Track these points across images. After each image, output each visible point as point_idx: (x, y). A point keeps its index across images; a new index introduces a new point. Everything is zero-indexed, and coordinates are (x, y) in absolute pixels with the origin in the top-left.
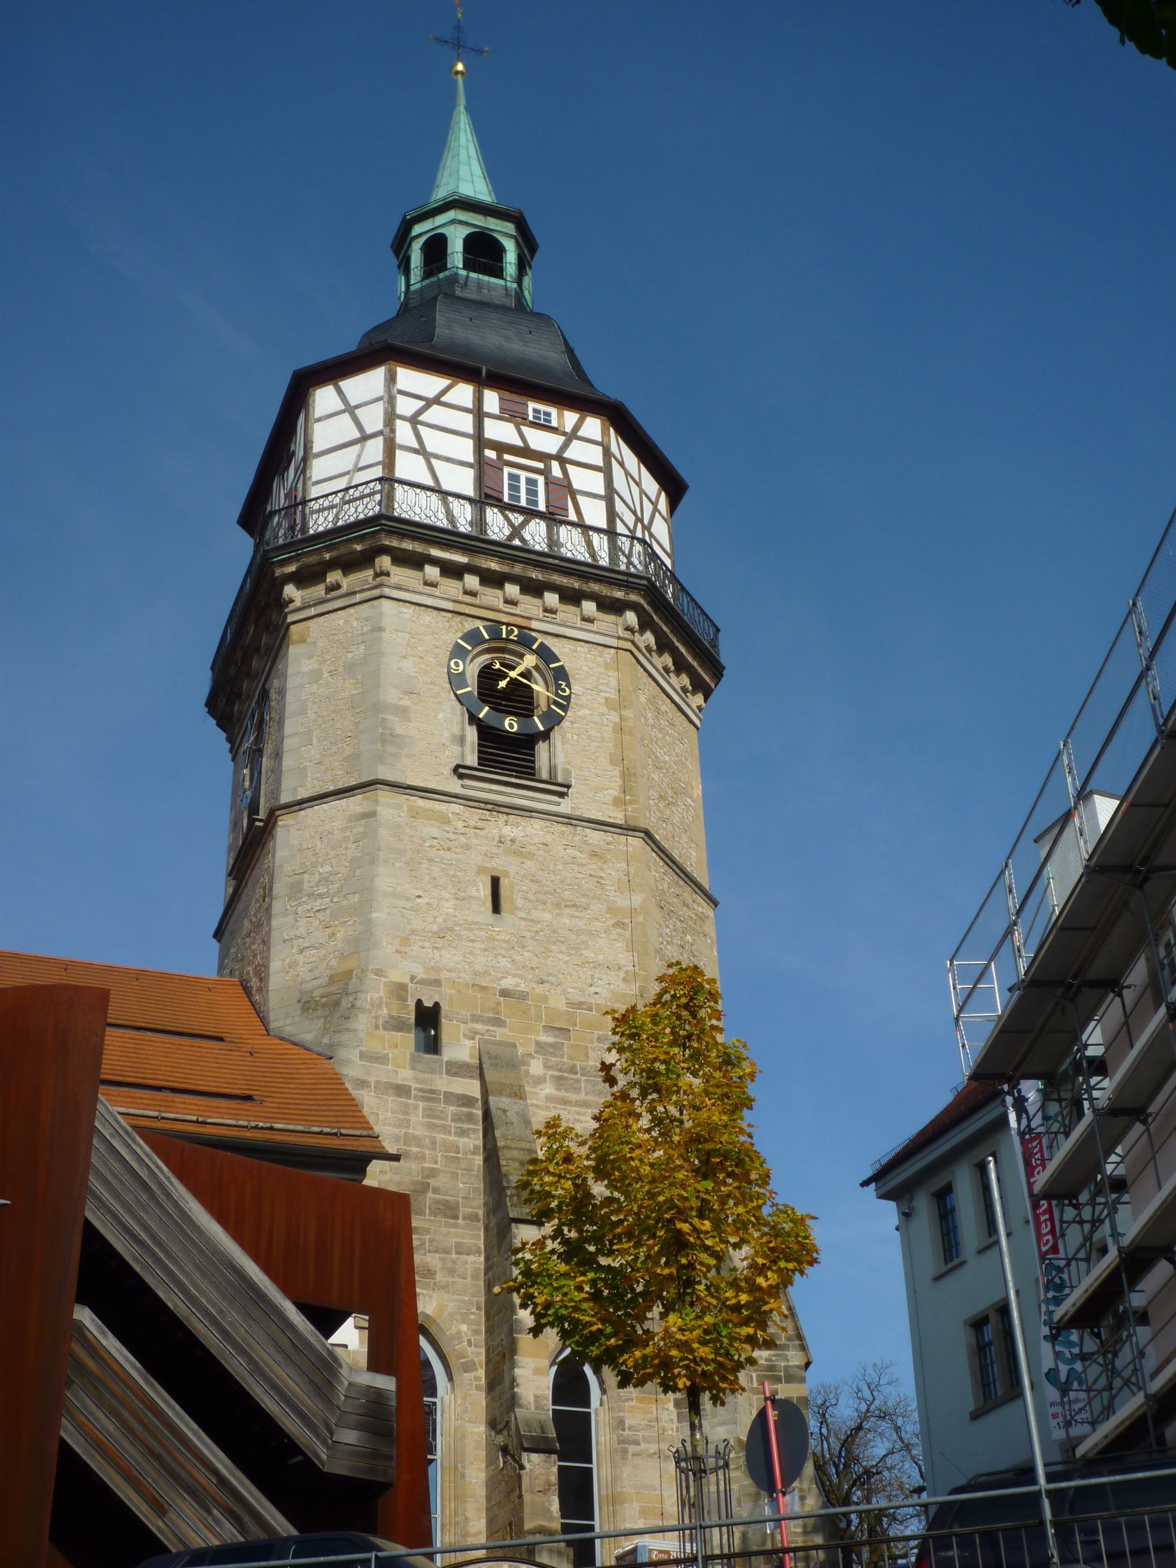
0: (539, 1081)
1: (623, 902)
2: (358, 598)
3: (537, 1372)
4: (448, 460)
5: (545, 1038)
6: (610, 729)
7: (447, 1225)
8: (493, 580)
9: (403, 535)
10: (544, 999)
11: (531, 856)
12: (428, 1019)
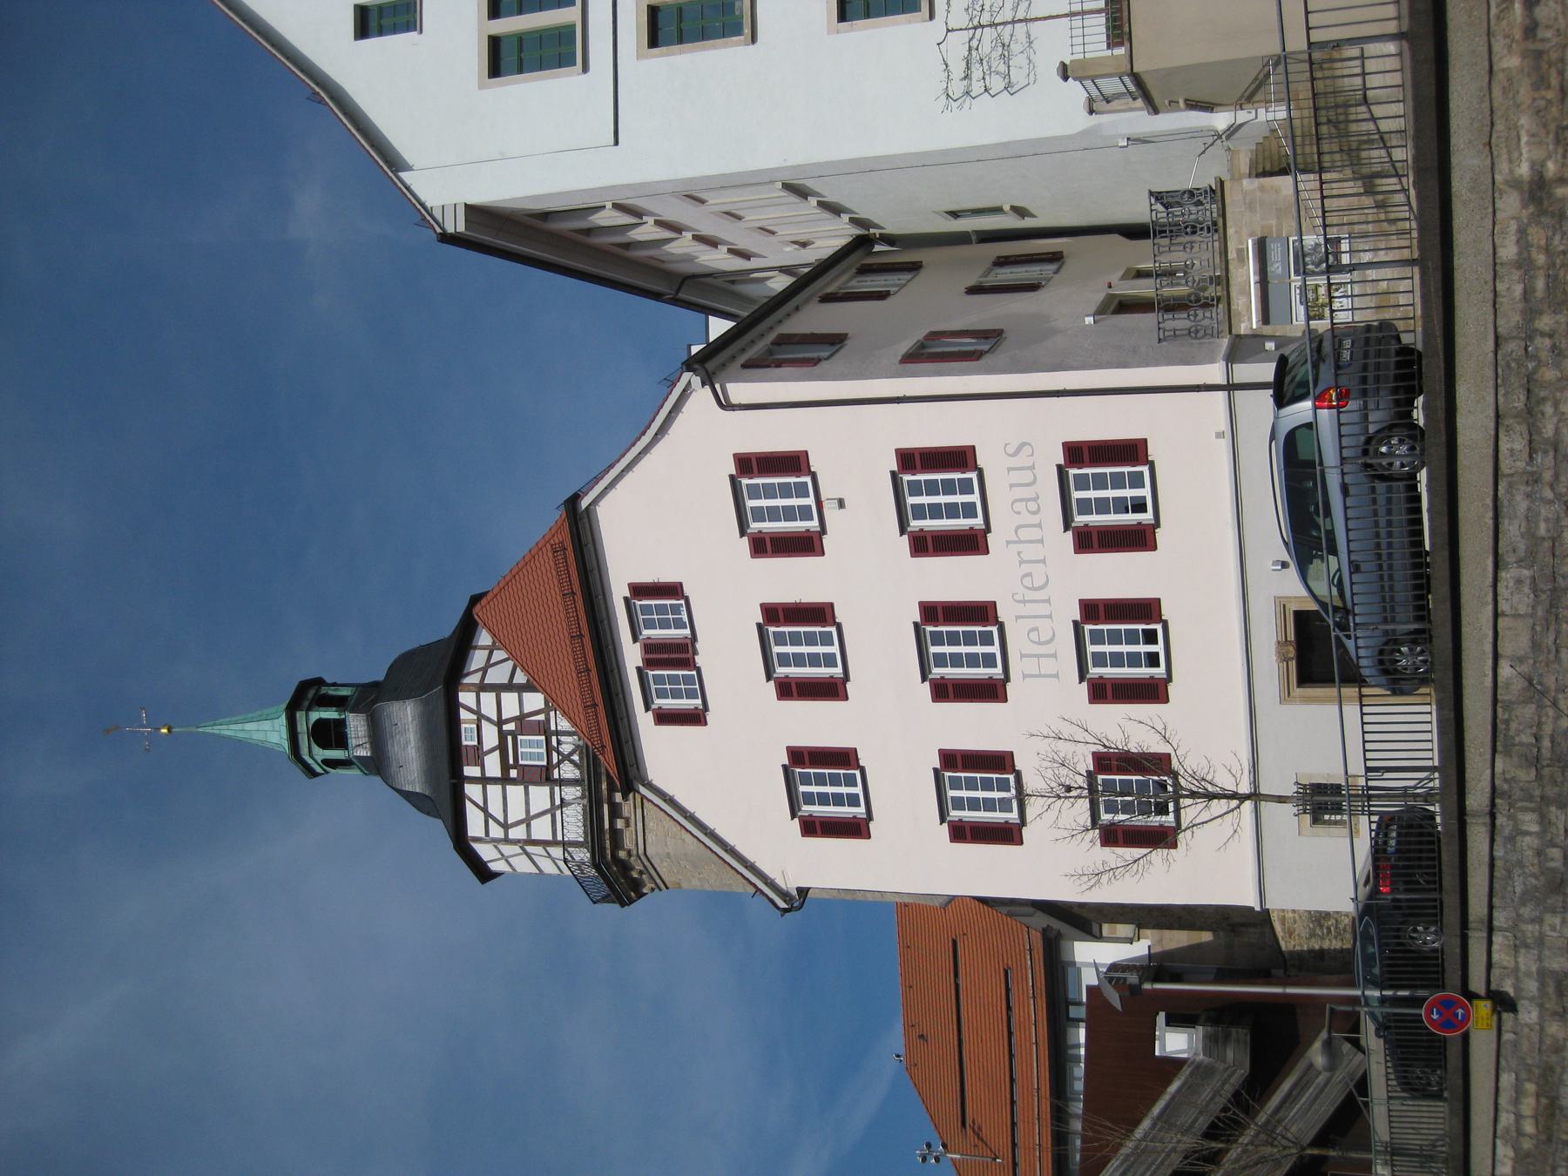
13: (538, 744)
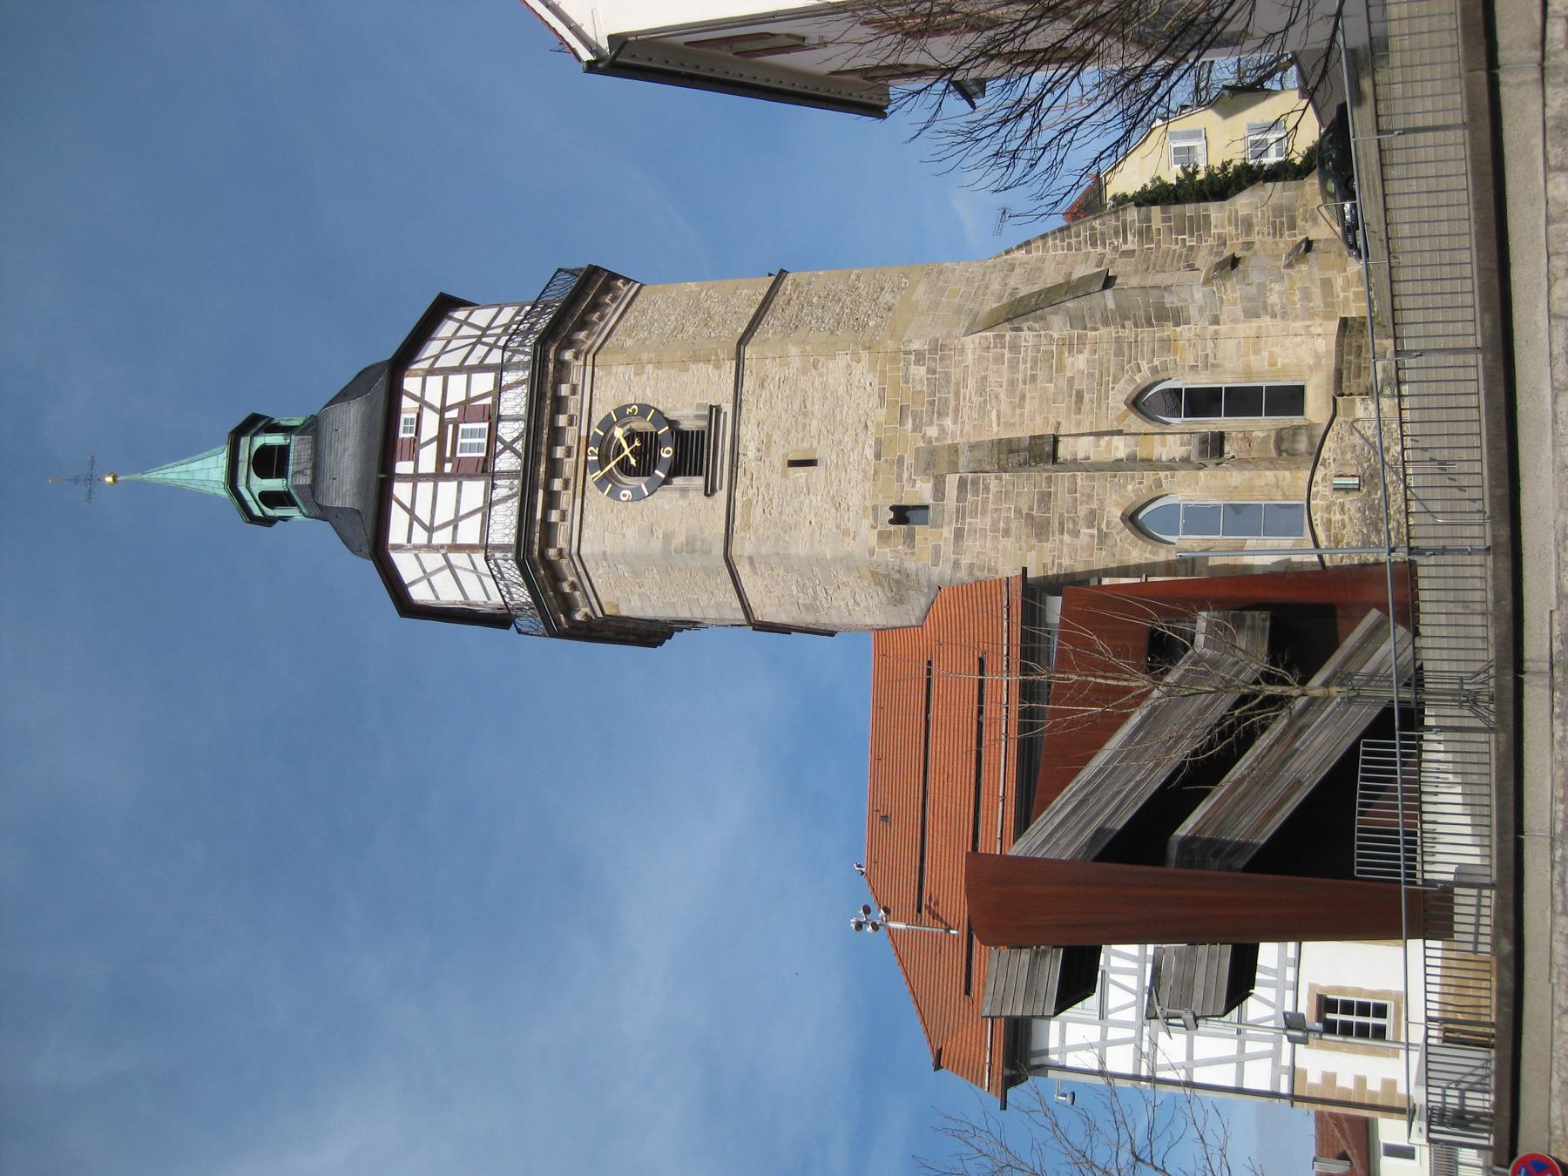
0: (942, 429)
1: (796, 363)
2: (580, 570)
3: (1164, 444)
4: (458, 502)
8: (554, 468)
9: (530, 542)
10: (879, 425)
11: (769, 436)
12: (902, 515)
13: (480, 433)
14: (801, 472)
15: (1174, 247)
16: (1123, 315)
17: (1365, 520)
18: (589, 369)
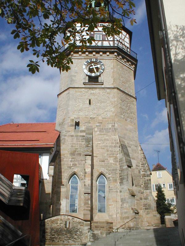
0: (97, 131)
1: (113, 100)
5: (98, 124)
6: (111, 72)
7: (79, 157)
8: (91, 52)
11: (96, 95)
12: (77, 124)
14: (88, 102)
15: (141, 182)
16: (122, 170)
17: (58, 229)
18: (113, 58)
